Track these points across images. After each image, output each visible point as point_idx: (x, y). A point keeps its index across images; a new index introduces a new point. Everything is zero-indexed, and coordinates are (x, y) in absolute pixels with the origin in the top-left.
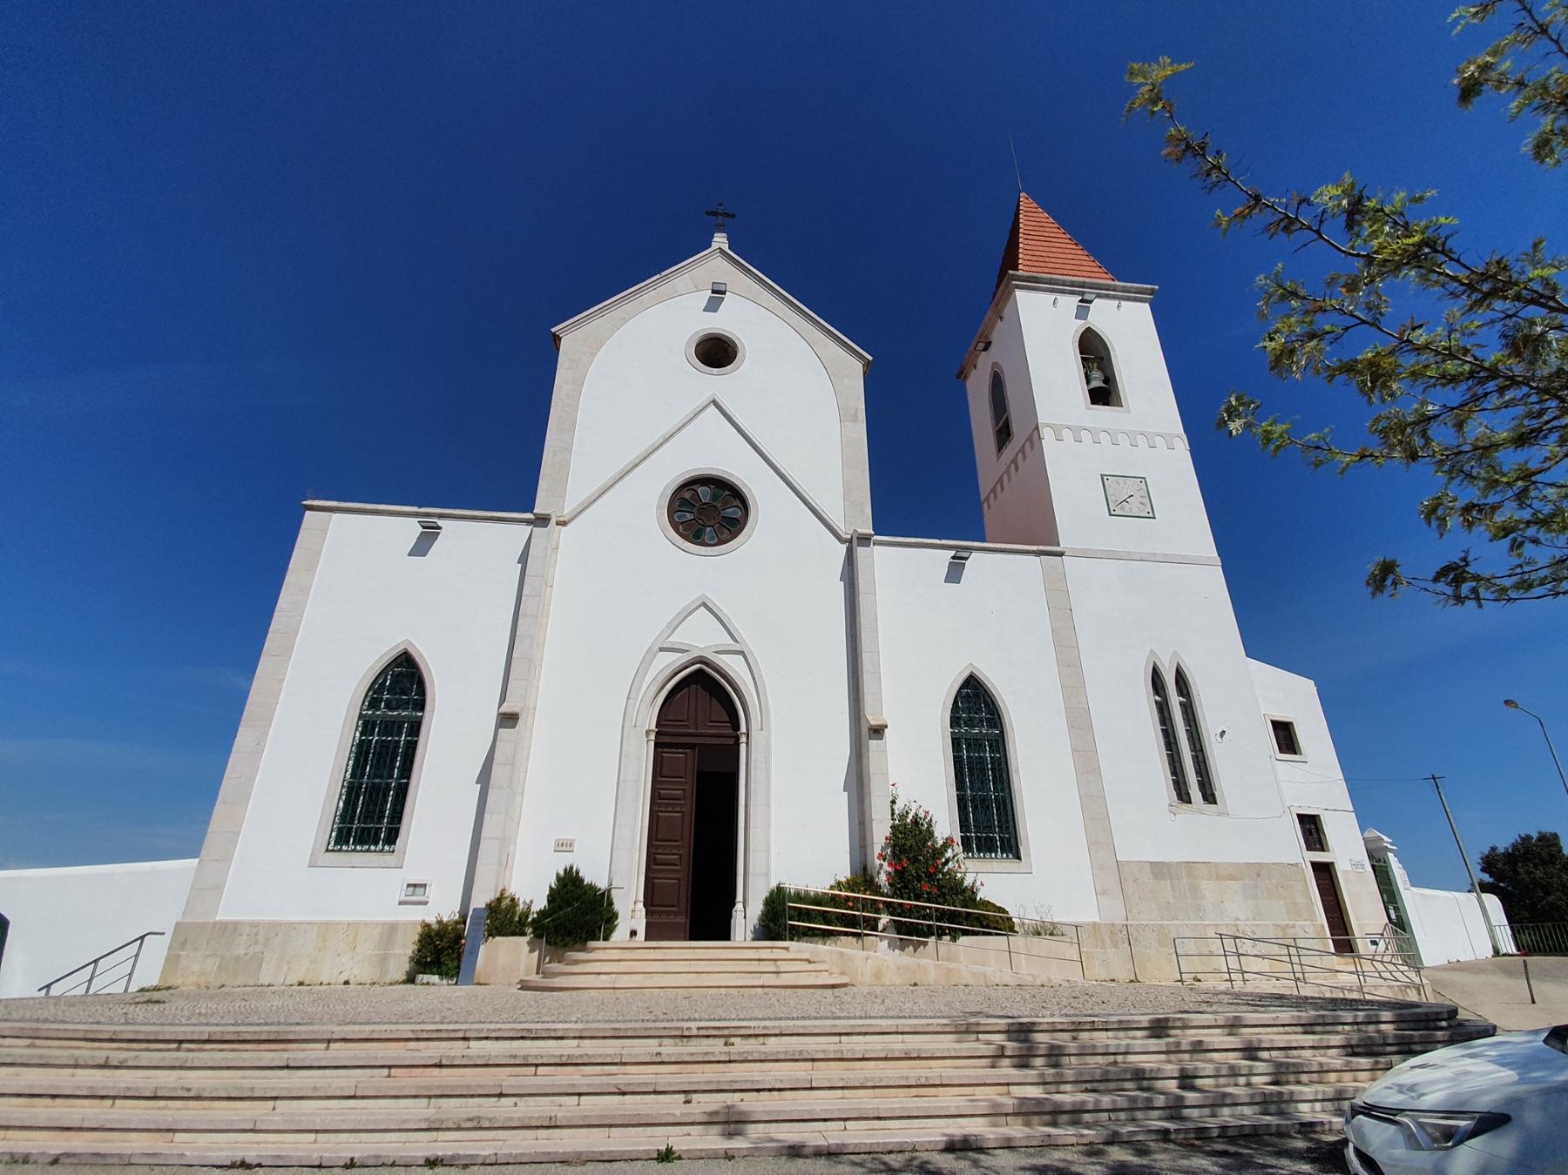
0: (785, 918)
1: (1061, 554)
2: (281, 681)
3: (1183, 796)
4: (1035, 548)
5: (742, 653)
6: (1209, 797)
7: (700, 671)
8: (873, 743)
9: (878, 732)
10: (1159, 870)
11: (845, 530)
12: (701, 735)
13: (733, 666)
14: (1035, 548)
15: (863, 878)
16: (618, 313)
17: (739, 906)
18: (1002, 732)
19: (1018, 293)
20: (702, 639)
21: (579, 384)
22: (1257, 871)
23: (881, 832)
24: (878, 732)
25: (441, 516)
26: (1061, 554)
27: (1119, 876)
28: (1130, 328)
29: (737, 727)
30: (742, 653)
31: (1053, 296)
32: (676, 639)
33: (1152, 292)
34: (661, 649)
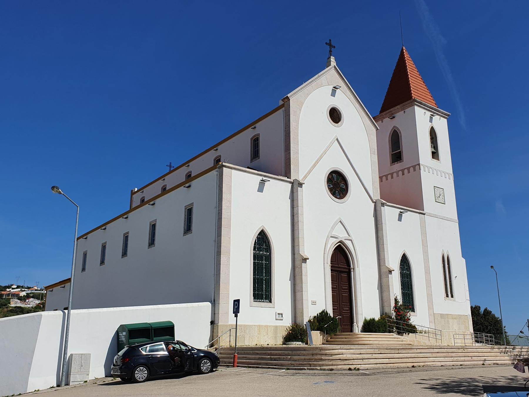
0: (370, 326)
1: (424, 214)
2: (230, 238)
3: (447, 296)
4: (418, 211)
5: (351, 240)
6: (452, 296)
7: (339, 245)
8: (390, 275)
9: (305, 260)
10: (442, 316)
11: (375, 199)
12: (339, 267)
13: (348, 243)
14: (418, 211)
15: (384, 315)
16: (305, 90)
17: (355, 323)
18: (270, 254)
19: (416, 107)
20: (342, 235)
21: (297, 122)
22: (460, 316)
23: (110, 380)
24: (305, 260)
25: (271, 178)
26: (424, 214)
27: (434, 317)
28: (441, 125)
29: (349, 266)
30: (351, 240)
31: (425, 111)
32: (334, 233)
33: (448, 115)
34: (331, 237)
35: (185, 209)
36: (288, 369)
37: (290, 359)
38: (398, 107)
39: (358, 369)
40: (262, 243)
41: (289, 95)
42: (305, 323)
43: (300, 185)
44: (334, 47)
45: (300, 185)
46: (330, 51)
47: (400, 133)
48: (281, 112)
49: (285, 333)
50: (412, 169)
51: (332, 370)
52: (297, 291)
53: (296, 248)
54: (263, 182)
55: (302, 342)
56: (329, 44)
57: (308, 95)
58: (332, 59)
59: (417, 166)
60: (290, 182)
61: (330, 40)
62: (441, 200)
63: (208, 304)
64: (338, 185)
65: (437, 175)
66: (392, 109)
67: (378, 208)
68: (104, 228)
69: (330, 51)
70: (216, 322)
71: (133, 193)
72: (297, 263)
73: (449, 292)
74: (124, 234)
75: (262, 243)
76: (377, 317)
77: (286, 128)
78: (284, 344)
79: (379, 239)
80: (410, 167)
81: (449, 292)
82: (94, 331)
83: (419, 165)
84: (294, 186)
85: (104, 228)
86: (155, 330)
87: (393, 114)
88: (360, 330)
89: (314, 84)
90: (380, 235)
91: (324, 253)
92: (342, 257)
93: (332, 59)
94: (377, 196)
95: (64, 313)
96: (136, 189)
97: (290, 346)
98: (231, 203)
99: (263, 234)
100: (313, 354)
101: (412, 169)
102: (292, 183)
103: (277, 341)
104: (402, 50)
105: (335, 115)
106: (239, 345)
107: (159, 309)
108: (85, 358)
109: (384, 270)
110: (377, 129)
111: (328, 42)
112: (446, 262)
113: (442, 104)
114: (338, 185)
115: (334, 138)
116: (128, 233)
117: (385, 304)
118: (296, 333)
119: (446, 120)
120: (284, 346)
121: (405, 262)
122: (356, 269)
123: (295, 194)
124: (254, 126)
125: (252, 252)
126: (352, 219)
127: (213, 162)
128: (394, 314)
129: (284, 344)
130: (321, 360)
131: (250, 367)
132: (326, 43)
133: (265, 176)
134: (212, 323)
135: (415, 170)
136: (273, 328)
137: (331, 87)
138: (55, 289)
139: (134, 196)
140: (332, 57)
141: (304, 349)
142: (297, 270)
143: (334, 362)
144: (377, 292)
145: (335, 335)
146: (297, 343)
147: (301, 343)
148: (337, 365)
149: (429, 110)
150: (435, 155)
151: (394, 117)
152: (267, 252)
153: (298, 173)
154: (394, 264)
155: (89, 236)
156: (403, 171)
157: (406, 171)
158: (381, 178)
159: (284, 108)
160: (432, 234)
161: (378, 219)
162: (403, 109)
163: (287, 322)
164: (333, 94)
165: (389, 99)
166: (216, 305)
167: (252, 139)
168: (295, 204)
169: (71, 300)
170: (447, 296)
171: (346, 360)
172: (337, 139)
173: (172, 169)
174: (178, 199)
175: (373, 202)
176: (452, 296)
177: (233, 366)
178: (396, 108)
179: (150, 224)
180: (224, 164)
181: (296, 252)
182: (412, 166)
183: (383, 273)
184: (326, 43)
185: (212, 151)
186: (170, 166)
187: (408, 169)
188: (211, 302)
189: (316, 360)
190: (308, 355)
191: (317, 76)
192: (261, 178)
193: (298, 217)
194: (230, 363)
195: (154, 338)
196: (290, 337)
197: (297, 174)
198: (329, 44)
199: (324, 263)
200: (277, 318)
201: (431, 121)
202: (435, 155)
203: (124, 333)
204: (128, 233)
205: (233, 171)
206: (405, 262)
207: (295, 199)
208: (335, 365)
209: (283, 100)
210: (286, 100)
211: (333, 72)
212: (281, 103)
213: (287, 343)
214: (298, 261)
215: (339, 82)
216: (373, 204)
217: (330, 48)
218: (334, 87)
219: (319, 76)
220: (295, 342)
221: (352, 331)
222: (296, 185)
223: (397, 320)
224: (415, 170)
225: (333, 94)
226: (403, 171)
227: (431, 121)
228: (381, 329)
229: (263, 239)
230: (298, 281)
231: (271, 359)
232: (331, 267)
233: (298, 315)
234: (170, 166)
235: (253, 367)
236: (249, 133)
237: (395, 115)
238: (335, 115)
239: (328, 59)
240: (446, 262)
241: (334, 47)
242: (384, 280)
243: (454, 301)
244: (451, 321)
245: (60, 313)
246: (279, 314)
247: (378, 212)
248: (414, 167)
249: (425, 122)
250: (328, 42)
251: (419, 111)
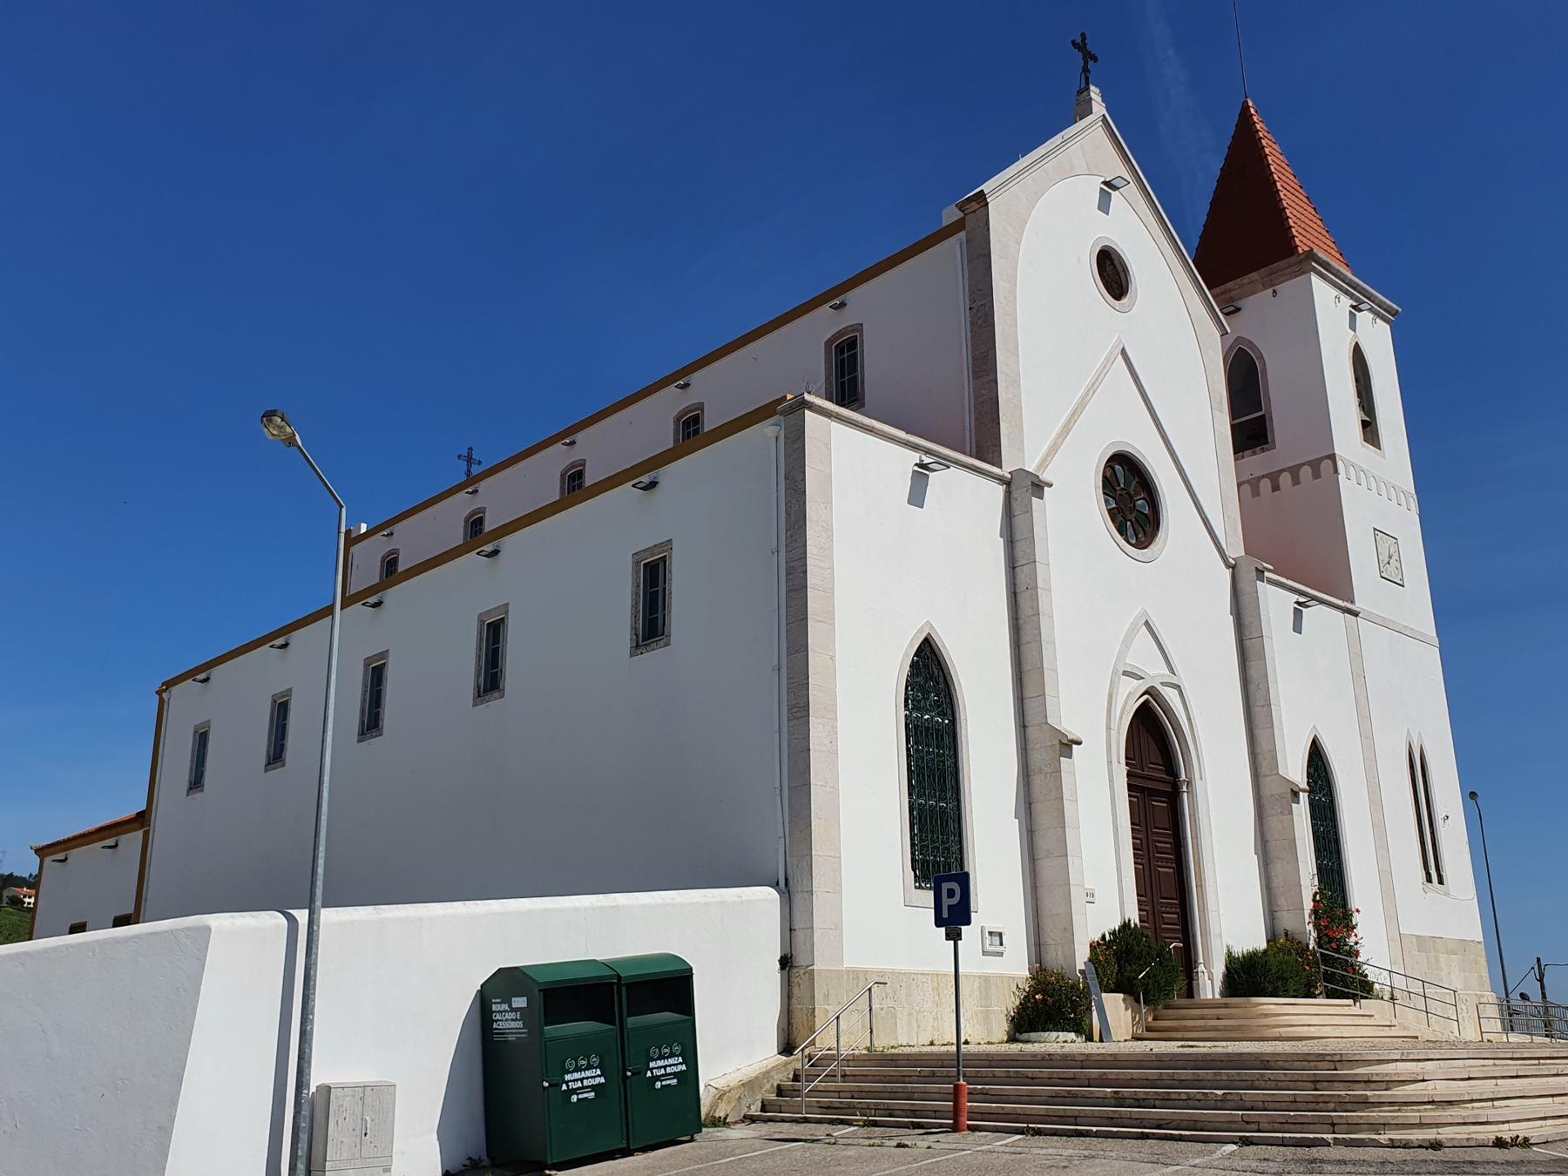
0: (1248, 977)
1: (1356, 614)
2: (832, 658)
3: (1429, 880)
5: (1178, 687)
6: (1441, 882)
13: (1171, 696)
17: (1201, 968)
20: (1155, 672)
24: (1067, 746)
26: (1356, 614)
28: (1378, 339)
31: (1335, 292)
32: (1132, 661)
34: (1125, 673)
35: (637, 563)
36: (1246, 1142)
37: (1224, 1097)
38: (1254, 275)
39: (1526, 1143)
40: (929, 678)
41: (986, 187)
42: (1080, 965)
43: (1038, 487)
44: (1095, 59)
45: (1038, 487)
46: (1086, 70)
47: (1261, 357)
48: (952, 248)
49: (1012, 1003)
50: (1306, 472)
51: (1436, 1145)
52: (1040, 853)
53: (1031, 705)
54: (921, 476)
55: (1078, 1032)
56: (1081, 46)
57: (1039, 195)
58: (1095, 93)
59: (1324, 463)
60: (1001, 480)
61: (1083, 36)
62: (1391, 572)
63: (766, 897)
64: (1131, 499)
65: (1377, 493)
66: (1230, 285)
67: (1244, 586)
68: (280, 641)
69: (1086, 70)
70: (800, 959)
71: (352, 540)
72: (1038, 758)
73: (1433, 870)
74: (368, 662)
75: (929, 678)
76: (1257, 941)
77: (973, 301)
78: (1012, 1039)
79: (1252, 688)
80: (1259, 479)
81: (1433, 870)
82: (402, 991)
83: (1332, 457)
84: (1015, 494)
85: (280, 641)
86: (629, 986)
87: (1232, 300)
88: (1217, 991)
89: (1050, 165)
90: (1253, 673)
91: (1109, 728)
92: (1153, 744)
93: (1095, 93)
94: (1236, 550)
95: (292, 921)
96: (364, 528)
97: (1028, 1048)
98: (830, 537)
99: (928, 651)
100: (1315, 1083)
101: (1306, 472)
102: (1007, 483)
103: (990, 1032)
104: (1246, 108)
105: (1112, 274)
106: (882, 1043)
107: (420, 919)
108: (376, 1097)
109: (1270, 788)
110: (1224, 333)
111: (1079, 40)
112: (1418, 770)
113: (1376, 277)
114: (1131, 499)
115: (1115, 347)
116: (383, 655)
117: (1282, 901)
118: (1048, 1004)
119: (1385, 329)
120: (1015, 1048)
121: (1317, 760)
122: (1198, 784)
123: (1019, 521)
124: (842, 298)
125: (903, 713)
126: (1139, 620)
127: (672, 427)
128: (1314, 934)
129: (1012, 1039)
130: (1365, 1103)
131: (1038, 1132)
132: (1073, 42)
133: (928, 452)
134: (786, 962)
135: (1316, 475)
136: (976, 985)
137: (1096, 183)
138: (75, 854)
139: (354, 549)
140: (1092, 88)
141: (1086, 1061)
142: (1037, 782)
143: (1411, 1115)
144: (1253, 861)
145: (1167, 1007)
146: (1063, 1036)
147: (1072, 1035)
148: (1438, 1125)
149: (1346, 292)
150: (1370, 429)
151: (1238, 310)
152: (943, 714)
153: (1021, 450)
154: (1295, 770)
155: (217, 673)
156: (1274, 478)
157: (1285, 479)
158: (1239, 485)
159: (962, 234)
160: (1369, 681)
161: (1247, 621)
162: (1270, 283)
163: (1016, 965)
164: (1104, 205)
165: (1237, 245)
166: (798, 899)
167: (828, 343)
168: (1019, 553)
169: (320, 870)
170: (1429, 880)
171: (1450, 1103)
172: (1123, 352)
173: (476, 470)
174: (613, 529)
175: (1228, 566)
176: (1441, 882)
177: (955, 1128)
178: (1246, 279)
179: (481, 622)
180: (807, 397)
181: (1032, 718)
182: (1309, 463)
183: (1267, 802)
184: (1073, 42)
185: (672, 388)
186: (470, 460)
187: (1294, 471)
188: (776, 885)
189: (1343, 1104)
190: (1293, 1084)
191: (1057, 139)
192: (915, 457)
193: (1035, 598)
194: (936, 1113)
195: (630, 1020)
196: (1027, 1020)
197: (1024, 444)
198: (1081, 46)
199: (1110, 762)
200: (988, 948)
201: (1353, 326)
202: (1370, 429)
203: (520, 1002)
204: (383, 655)
205: (835, 426)
206: (1317, 760)
207: (1018, 537)
208: (1429, 1125)
209: (961, 207)
210: (974, 206)
211: (1099, 133)
212: (951, 215)
213: (1025, 1036)
214: (1041, 751)
215: (1115, 167)
216: (1228, 572)
217: (1086, 63)
218: (1105, 183)
219: (1065, 142)
220: (1054, 1034)
221: (1190, 993)
222: (1022, 491)
223: (1315, 957)
224: (1316, 475)
225: (1104, 205)
226: (1274, 478)
227: (1353, 326)
228: (1291, 985)
229: (926, 667)
230: (1043, 821)
231: (1120, 1101)
232: (1129, 775)
233: (1051, 936)
234: (470, 460)
235: (1055, 1133)
236: (823, 325)
237: (1238, 304)
238: (1112, 274)
239: (1080, 92)
240: (1418, 770)
241: (1095, 59)
242: (1274, 823)
243: (1447, 894)
244: (1443, 958)
245: (273, 921)
246: (991, 933)
247: (1246, 600)
248: (1315, 465)
249: (1342, 329)
250: (1079, 40)
251: (1322, 292)
